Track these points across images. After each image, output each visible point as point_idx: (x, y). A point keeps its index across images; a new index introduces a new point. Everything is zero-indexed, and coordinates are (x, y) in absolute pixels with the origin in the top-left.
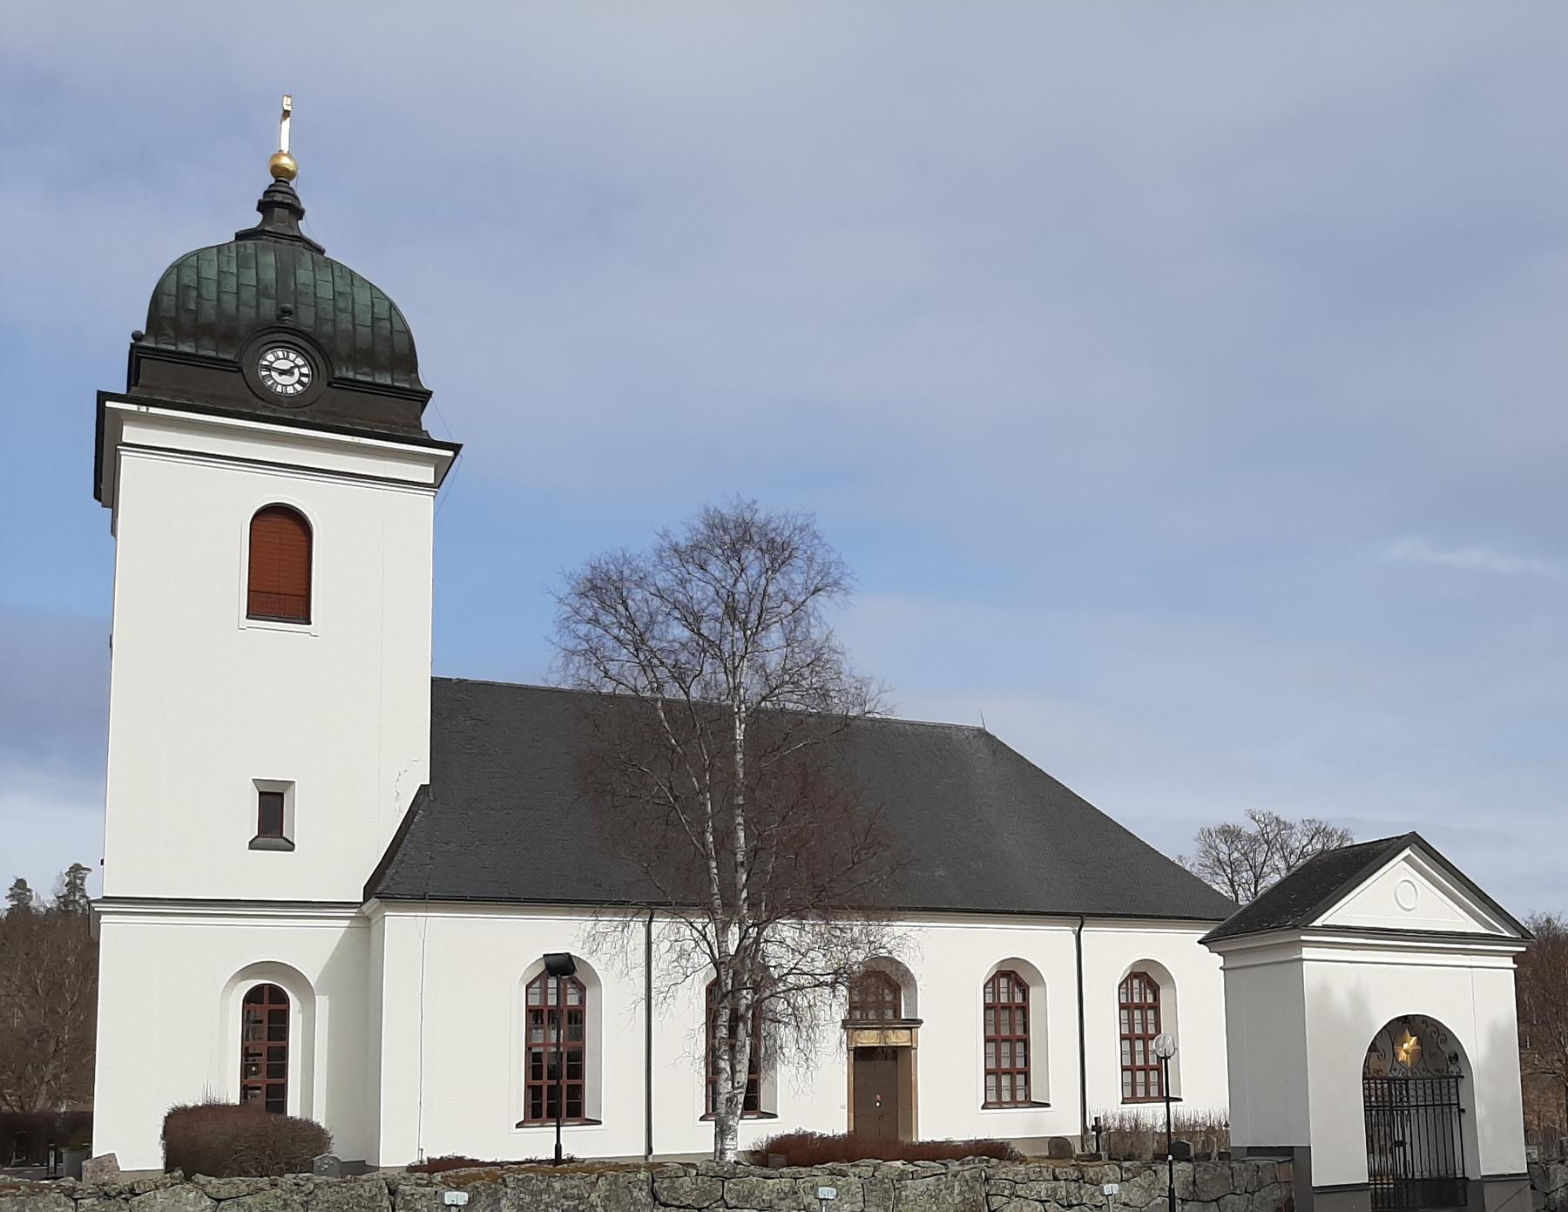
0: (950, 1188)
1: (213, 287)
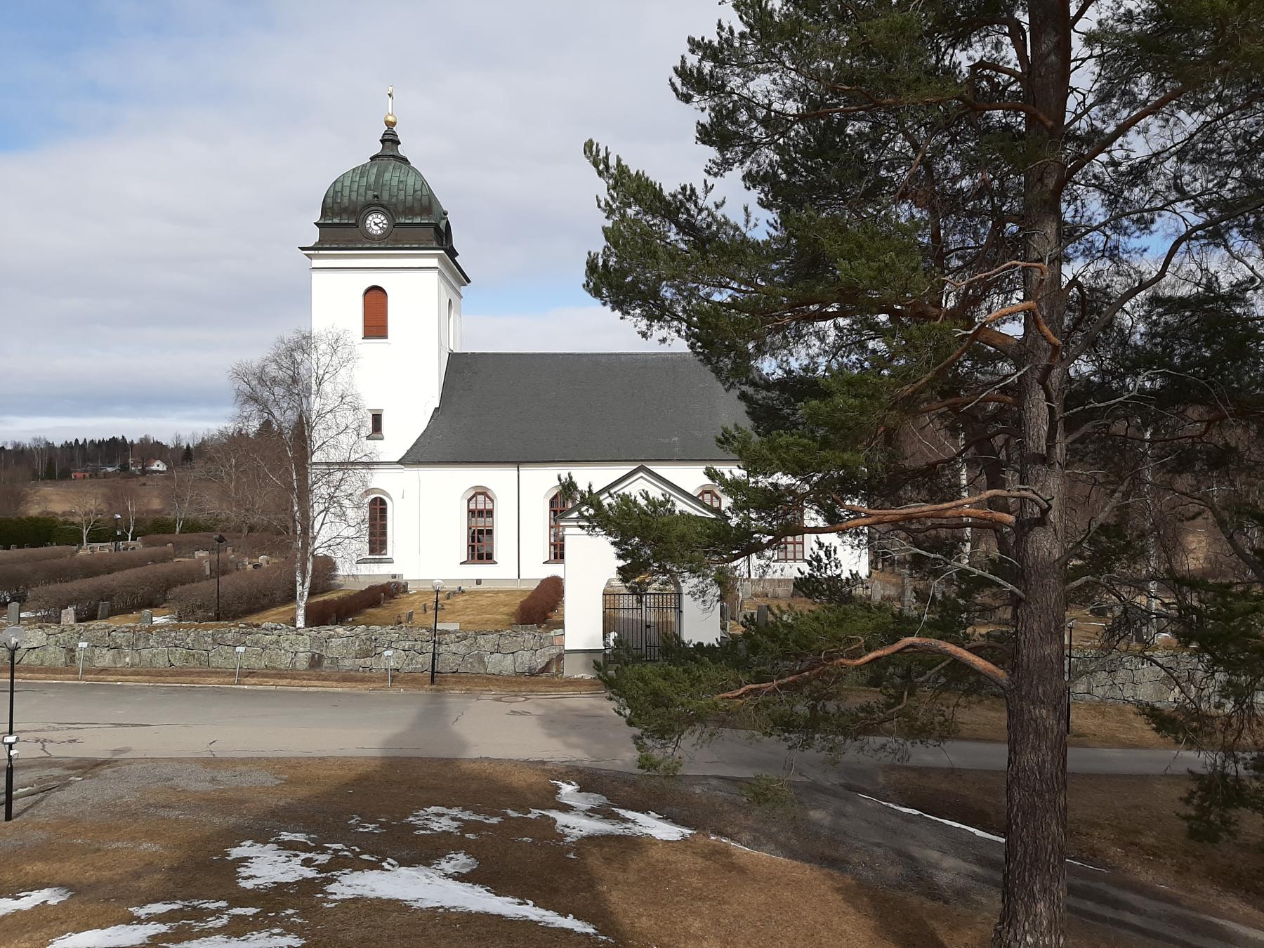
0: (354, 643)
1: (348, 189)
